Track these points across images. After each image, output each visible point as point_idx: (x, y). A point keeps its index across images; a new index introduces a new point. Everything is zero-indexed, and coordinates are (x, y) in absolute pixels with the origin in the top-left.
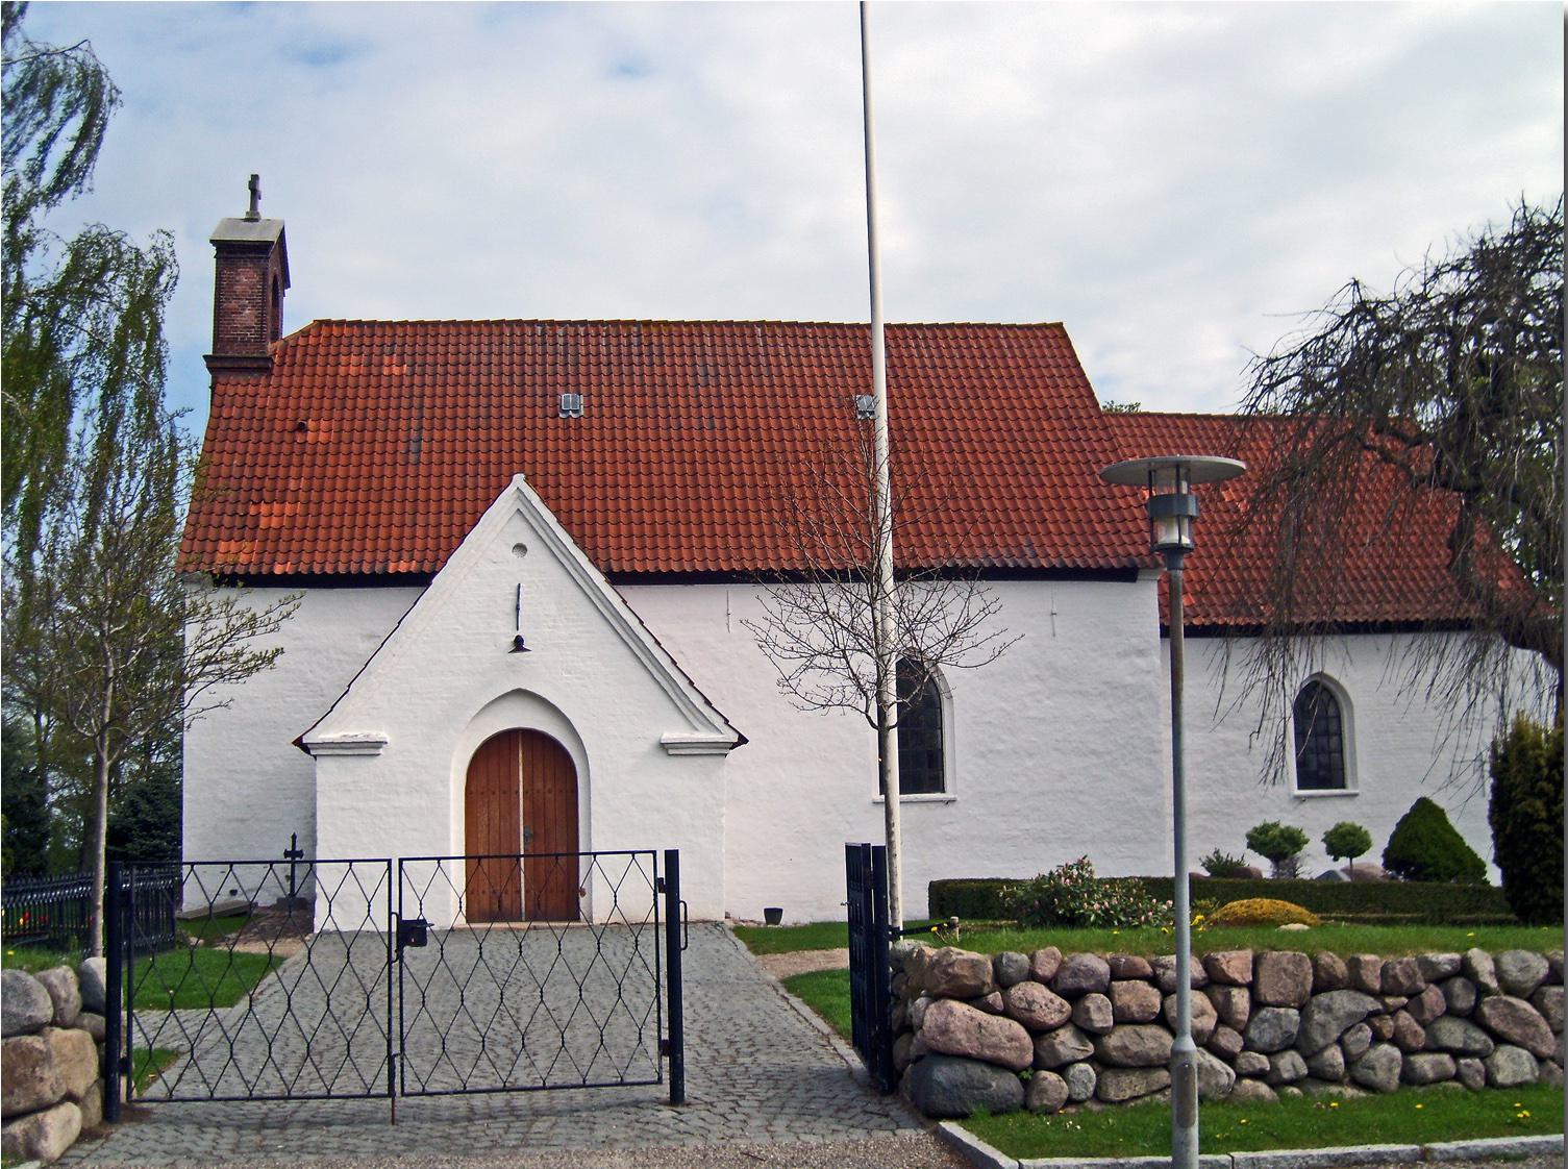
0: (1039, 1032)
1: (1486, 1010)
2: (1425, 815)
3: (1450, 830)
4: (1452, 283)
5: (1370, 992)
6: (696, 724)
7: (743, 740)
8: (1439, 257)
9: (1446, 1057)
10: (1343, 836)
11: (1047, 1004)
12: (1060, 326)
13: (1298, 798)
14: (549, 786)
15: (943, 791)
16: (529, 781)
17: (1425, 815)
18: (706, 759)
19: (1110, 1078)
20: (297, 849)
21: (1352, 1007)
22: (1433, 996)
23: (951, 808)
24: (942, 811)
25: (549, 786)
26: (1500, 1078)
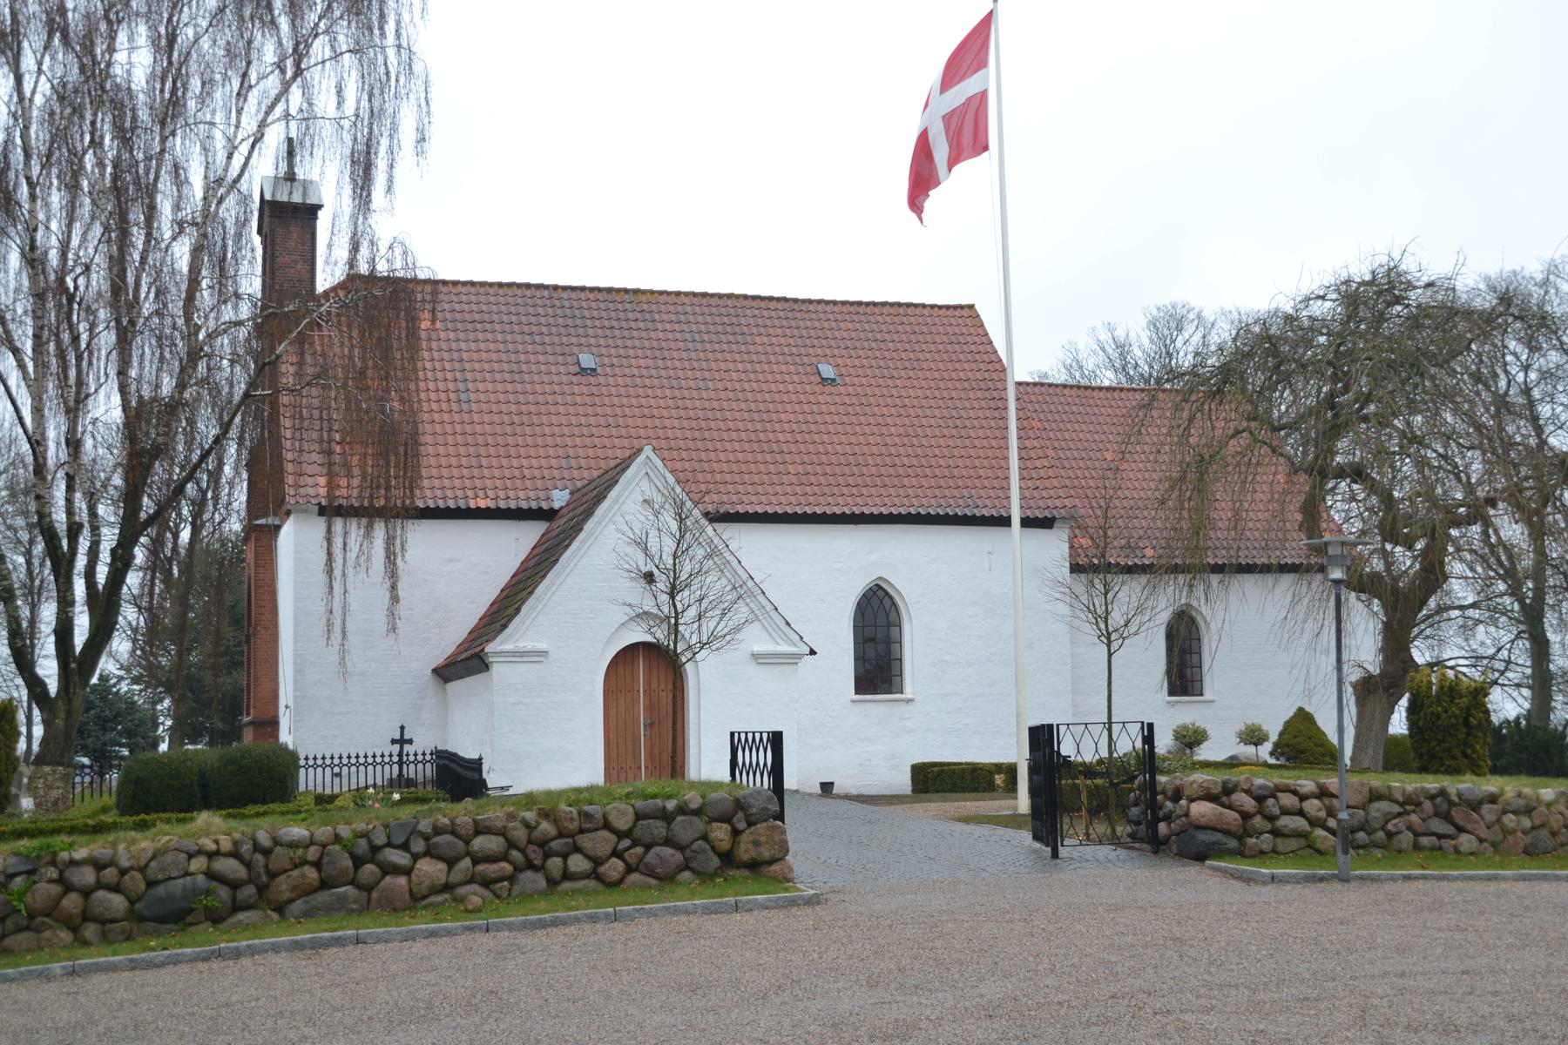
0: (1246, 816)
1: (1453, 813)
2: (1303, 719)
3: (1318, 729)
4: (1320, 309)
5: (1397, 802)
6: (778, 640)
7: (813, 652)
8: (1306, 289)
9: (1434, 838)
10: (1253, 731)
11: (1248, 803)
12: (971, 307)
13: (1169, 702)
14: (662, 686)
15: (902, 692)
16: (648, 683)
17: (1303, 719)
18: (784, 667)
19: (1279, 840)
20: (406, 737)
21: (1389, 809)
22: (1427, 805)
23: (910, 707)
24: (903, 708)
25: (662, 686)
26: (1462, 849)
